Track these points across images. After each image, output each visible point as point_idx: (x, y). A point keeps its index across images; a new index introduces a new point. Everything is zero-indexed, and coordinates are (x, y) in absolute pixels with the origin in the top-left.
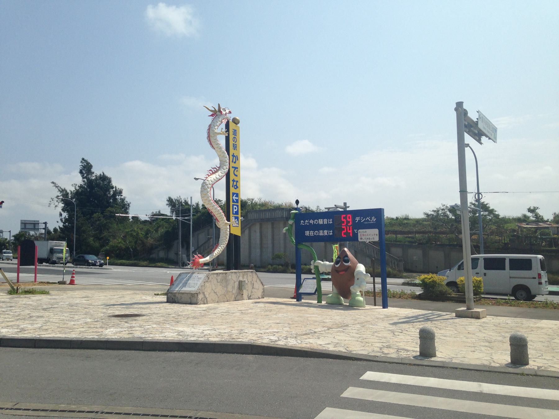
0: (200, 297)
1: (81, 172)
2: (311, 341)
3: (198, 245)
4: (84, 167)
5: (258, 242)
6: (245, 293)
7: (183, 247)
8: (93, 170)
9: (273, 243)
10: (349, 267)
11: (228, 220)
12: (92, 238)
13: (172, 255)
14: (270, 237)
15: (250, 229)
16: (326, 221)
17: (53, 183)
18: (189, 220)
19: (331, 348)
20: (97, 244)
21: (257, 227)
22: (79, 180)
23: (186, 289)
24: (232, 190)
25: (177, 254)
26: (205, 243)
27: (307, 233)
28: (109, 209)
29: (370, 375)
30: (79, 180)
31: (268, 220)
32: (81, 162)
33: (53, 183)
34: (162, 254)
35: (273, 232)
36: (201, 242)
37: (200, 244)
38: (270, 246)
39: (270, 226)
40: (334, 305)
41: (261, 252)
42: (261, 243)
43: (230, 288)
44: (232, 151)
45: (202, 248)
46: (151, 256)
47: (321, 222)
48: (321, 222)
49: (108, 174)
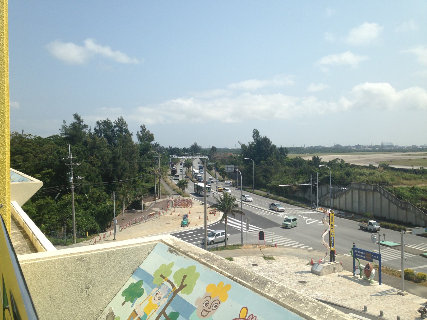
0: (321, 273)
1: (253, 137)
2: (344, 302)
3: (322, 194)
5: (357, 200)
6: (336, 271)
7: (313, 193)
8: (260, 135)
9: (366, 202)
10: (369, 270)
13: (306, 196)
14: (364, 198)
16: (363, 253)
18: (316, 185)
19: (347, 306)
22: (252, 140)
24: (331, 236)
26: (326, 195)
27: (357, 255)
30: (252, 140)
31: (363, 190)
33: (239, 142)
36: (324, 193)
37: (324, 194)
38: (364, 203)
41: (359, 205)
42: (359, 199)
43: (331, 270)
45: (324, 197)
46: (295, 195)
47: (361, 253)
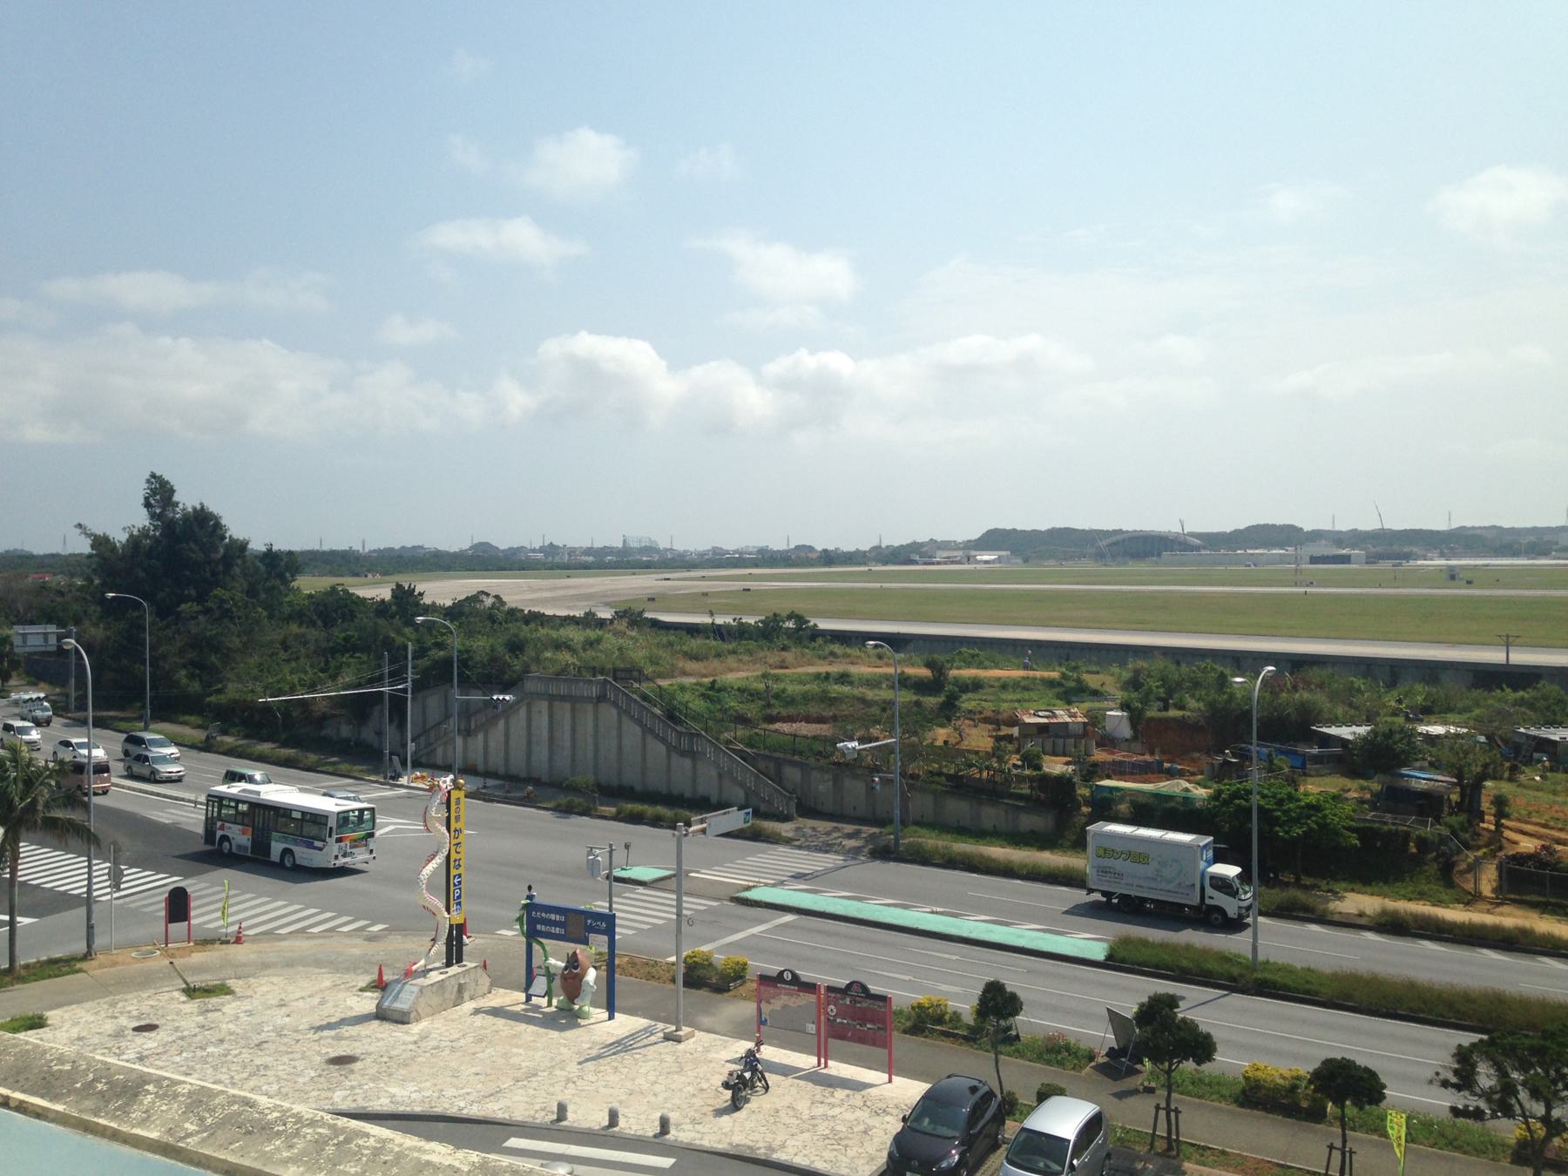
1: (147, 505)
4: (154, 492)
5: (545, 733)
7: (391, 721)
8: (176, 498)
11: (448, 910)
12: (184, 672)
13: (368, 734)
15: (529, 705)
17: (80, 526)
18: (405, 690)
19: (500, 1115)
20: (195, 687)
21: (544, 705)
22: (140, 519)
23: (397, 1005)
24: (453, 872)
25: (379, 734)
28: (218, 592)
29: (513, 1142)
30: (140, 519)
31: (563, 698)
32: (148, 481)
34: (346, 731)
35: (573, 717)
38: (568, 744)
39: (567, 706)
40: (549, 1022)
42: (551, 739)
43: (447, 995)
44: (453, 825)
45: (432, 734)
46: (323, 733)
47: (553, 917)
48: (553, 917)
49: (213, 507)
